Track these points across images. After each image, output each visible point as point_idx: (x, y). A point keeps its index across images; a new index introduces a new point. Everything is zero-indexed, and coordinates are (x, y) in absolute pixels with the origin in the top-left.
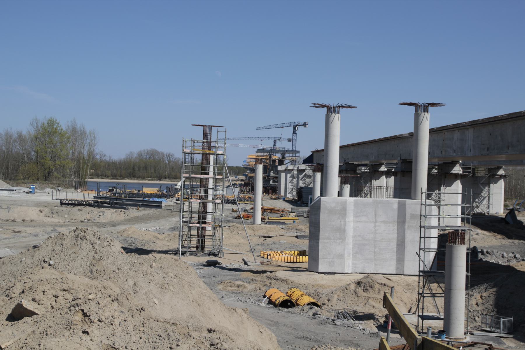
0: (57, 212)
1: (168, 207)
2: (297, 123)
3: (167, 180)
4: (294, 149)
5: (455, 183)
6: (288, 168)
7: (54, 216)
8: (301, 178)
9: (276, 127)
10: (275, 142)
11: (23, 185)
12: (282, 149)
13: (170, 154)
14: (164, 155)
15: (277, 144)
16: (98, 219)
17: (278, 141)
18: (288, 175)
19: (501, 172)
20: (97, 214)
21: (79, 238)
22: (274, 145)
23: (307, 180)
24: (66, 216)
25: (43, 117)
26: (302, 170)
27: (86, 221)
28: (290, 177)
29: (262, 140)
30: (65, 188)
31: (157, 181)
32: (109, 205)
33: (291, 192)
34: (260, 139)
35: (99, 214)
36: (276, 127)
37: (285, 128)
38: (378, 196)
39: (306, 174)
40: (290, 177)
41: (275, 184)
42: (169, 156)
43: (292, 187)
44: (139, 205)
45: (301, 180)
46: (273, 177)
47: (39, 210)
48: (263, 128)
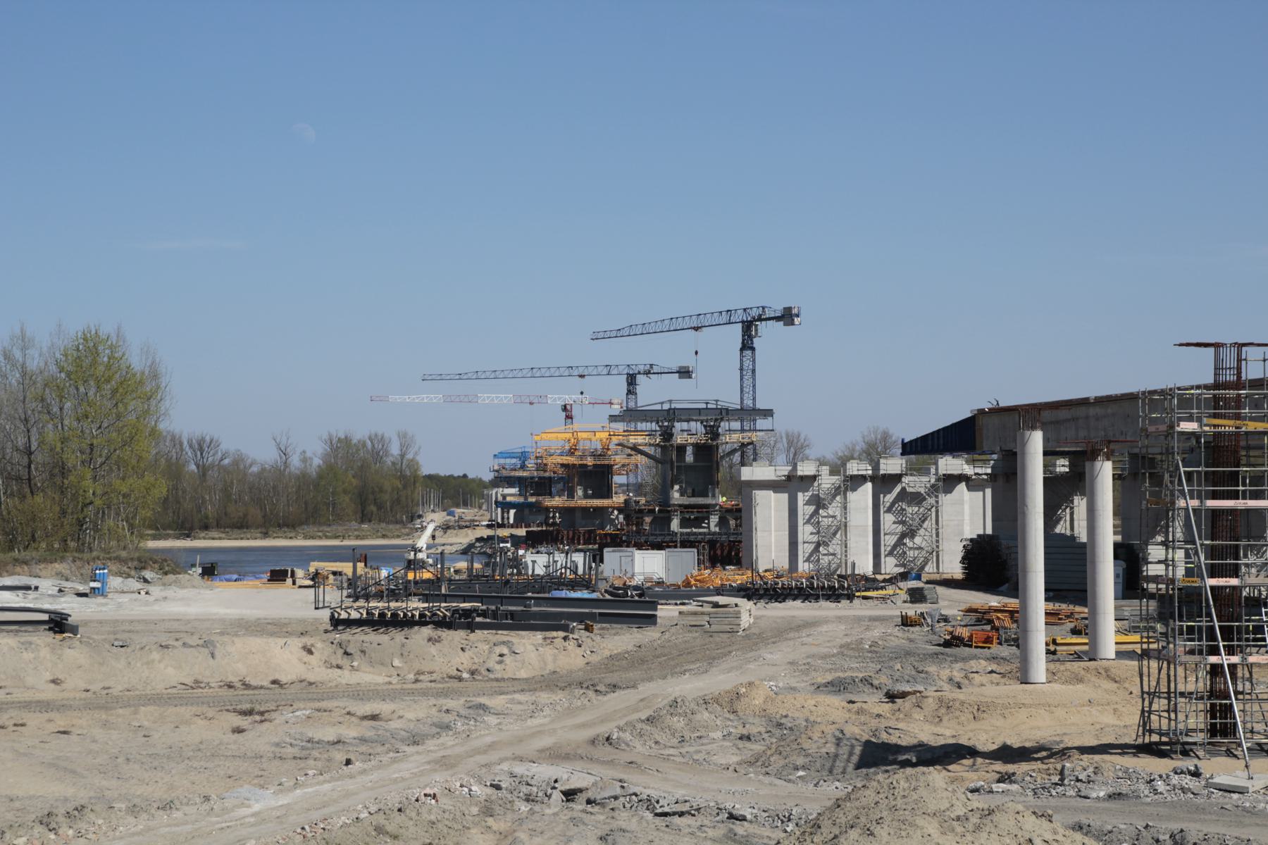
0: (363, 652)
1: (690, 618)
2: (755, 313)
3: (215, 534)
4: (748, 403)
6: (799, 473)
7: (355, 664)
8: (888, 505)
9: (672, 326)
10: (632, 380)
11: (18, 569)
12: (704, 406)
13: (203, 440)
14: (181, 444)
15: (639, 389)
16: (498, 667)
17: (640, 379)
18: (802, 498)
20: (490, 652)
21: (1113, 707)
22: (629, 392)
23: (910, 510)
24: (397, 663)
25: (75, 326)
26: (890, 475)
27: (465, 675)
28: (808, 503)
29: (582, 376)
30: (166, 573)
31: (178, 538)
32: (485, 617)
33: (811, 555)
34: (576, 373)
35: (498, 650)
36: (672, 326)
37: (704, 329)
38: (1222, 549)
39: (903, 489)
40: (808, 503)
41: (689, 530)
42: (201, 446)
43: (815, 538)
44: (592, 617)
45: (889, 510)
46: (680, 506)
47: (300, 645)
48: (619, 334)
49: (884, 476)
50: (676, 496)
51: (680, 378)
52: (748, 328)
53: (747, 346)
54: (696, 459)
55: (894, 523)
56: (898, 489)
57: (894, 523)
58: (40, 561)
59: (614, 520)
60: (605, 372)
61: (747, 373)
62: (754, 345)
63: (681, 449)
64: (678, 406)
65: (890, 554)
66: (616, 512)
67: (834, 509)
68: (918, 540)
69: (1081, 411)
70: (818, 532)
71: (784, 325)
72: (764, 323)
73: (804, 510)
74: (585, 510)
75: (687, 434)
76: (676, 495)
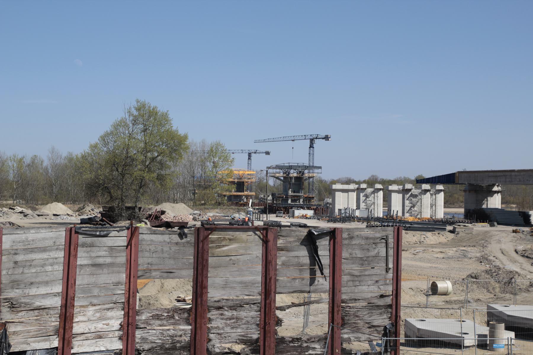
2: (315, 136)
4: (311, 164)
5: (441, 193)
8: (407, 198)
12: (297, 165)
15: (252, 158)
17: (253, 155)
19: (495, 189)
22: (249, 159)
25: (210, 140)
28: (364, 196)
39: (412, 193)
40: (364, 196)
45: (407, 199)
46: (291, 196)
49: (407, 189)
50: (290, 193)
51: (266, 155)
52: (312, 141)
53: (311, 146)
54: (295, 182)
55: (409, 203)
56: (410, 193)
57: (409, 203)
58: (211, 209)
59: (243, 199)
60: (241, 152)
61: (311, 155)
62: (314, 146)
63: (291, 178)
64: (293, 165)
65: (408, 212)
66: (244, 197)
67: (371, 198)
68: (415, 209)
69: (507, 174)
70: (366, 205)
71: (325, 140)
72: (318, 140)
73: (362, 198)
74: (234, 195)
75: (294, 174)
76: (290, 192)
